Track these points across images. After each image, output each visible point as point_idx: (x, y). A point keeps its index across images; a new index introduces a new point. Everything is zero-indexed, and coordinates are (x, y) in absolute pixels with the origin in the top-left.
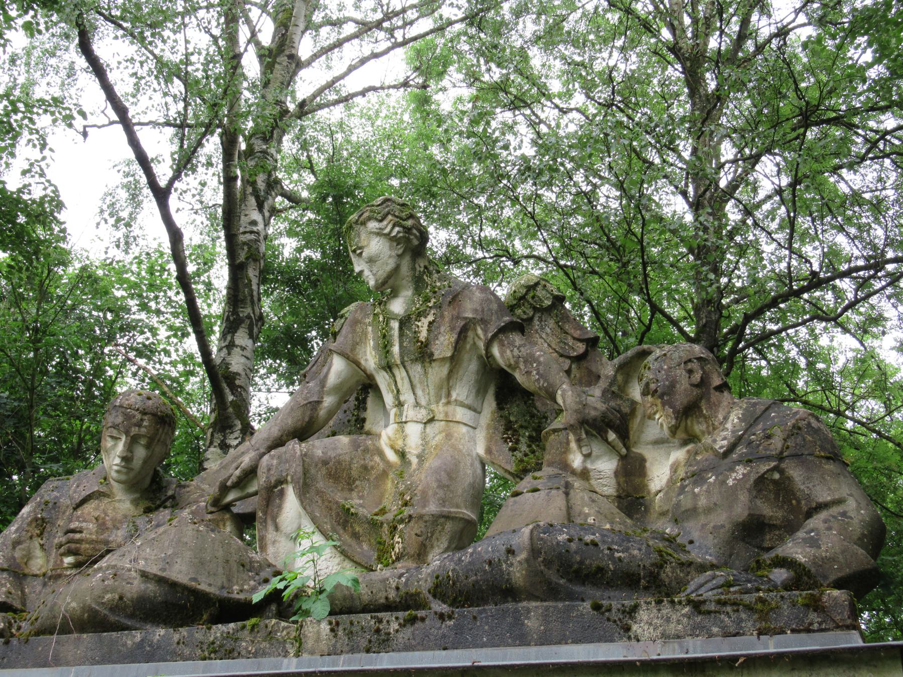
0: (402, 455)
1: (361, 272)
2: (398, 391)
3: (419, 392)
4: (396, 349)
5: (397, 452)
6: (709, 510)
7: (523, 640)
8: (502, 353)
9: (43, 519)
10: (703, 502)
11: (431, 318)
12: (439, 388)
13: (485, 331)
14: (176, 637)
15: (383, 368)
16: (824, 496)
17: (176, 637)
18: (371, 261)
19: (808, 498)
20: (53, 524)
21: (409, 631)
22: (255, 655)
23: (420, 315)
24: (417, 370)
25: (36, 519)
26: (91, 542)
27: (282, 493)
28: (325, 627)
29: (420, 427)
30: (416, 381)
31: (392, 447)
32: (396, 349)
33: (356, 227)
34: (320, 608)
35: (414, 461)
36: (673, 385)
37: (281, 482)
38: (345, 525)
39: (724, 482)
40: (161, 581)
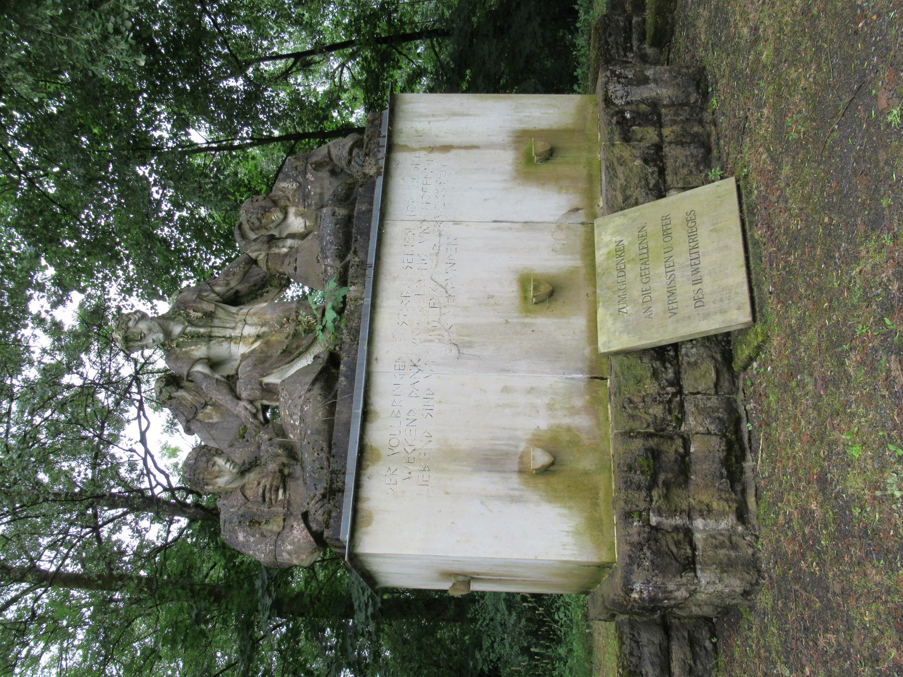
0: (258, 337)
1: (237, 81)
2: (224, 337)
3: (228, 325)
4: (202, 330)
5: (255, 341)
6: (322, 188)
7: (370, 211)
8: (220, 286)
9: (250, 522)
10: (318, 190)
11: (191, 311)
12: (229, 316)
13: (206, 291)
14: (346, 358)
15: (210, 341)
16: (326, 151)
17: (346, 358)
18: (150, 330)
19: (325, 157)
20: (255, 514)
21: (359, 253)
22: (360, 319)
23: (188, 315)
24: (216, 322)
25: (249, 525)
26: (273, 480)
27: (267, 384)
28: (352, 288)
29: (247, 327)
30: (221, 325)
31: (253, 343)
32: (202, 330)
33: (128, 334)
34: (343, 291)
35: (264, 329)
36: (261, 206)
37: (261, 383)
38: (291, 353)
39: (312, 182)
40: (313, 383)
